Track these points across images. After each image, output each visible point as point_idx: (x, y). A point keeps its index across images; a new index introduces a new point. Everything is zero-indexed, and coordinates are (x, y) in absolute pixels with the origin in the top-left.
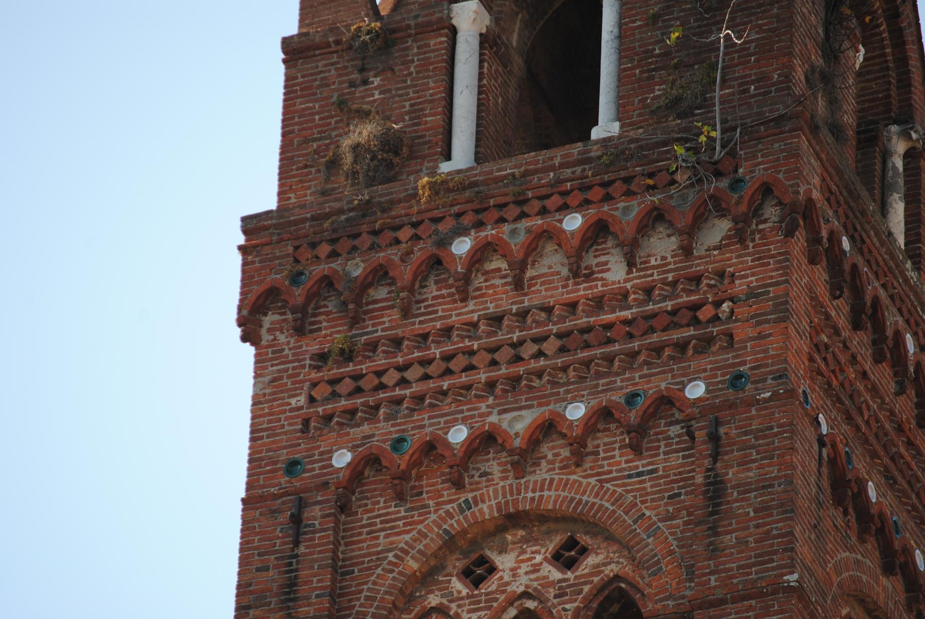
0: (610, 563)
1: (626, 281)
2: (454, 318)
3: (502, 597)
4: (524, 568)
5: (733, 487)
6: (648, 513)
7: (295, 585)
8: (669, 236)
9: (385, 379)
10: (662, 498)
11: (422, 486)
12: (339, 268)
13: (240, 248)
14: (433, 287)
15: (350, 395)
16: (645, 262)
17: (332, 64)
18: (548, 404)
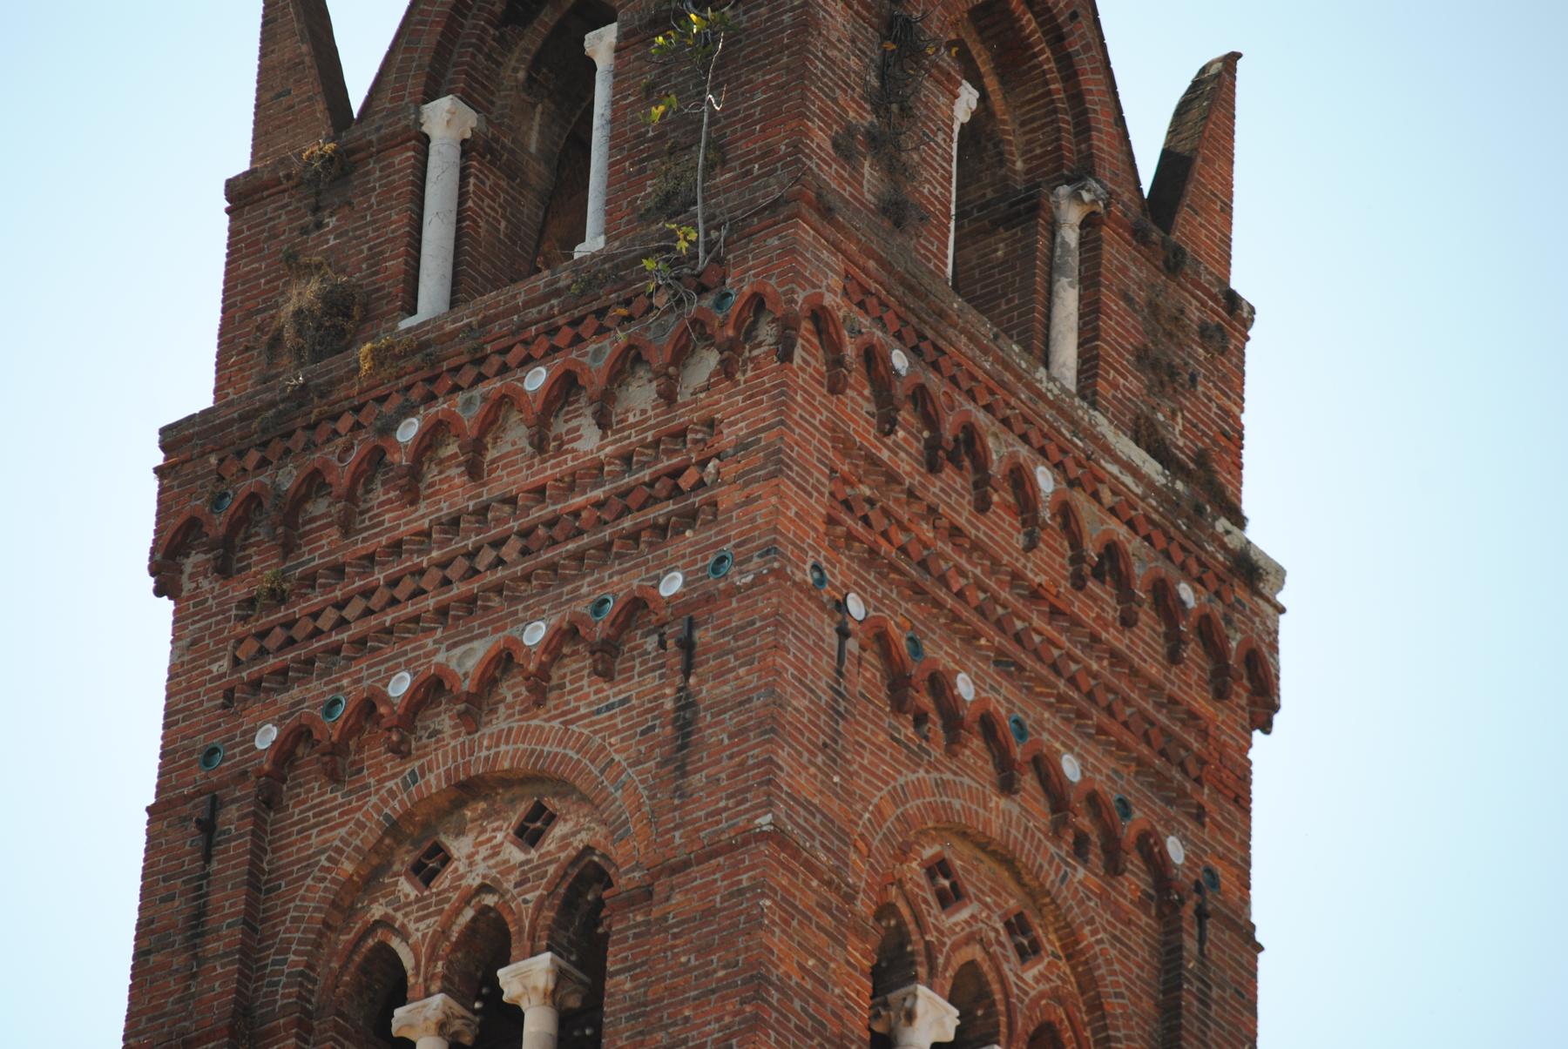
0: (579, 832)
1: (601, 448)
2: (402, 529)
3: (455, 896)
4: (484, 851)
5: (707, 709)
6: (617, 758)
7: (204, 914)
8: (650, 381)
9: (320, 623)
10: (632, 737)
11: (362, 760)
12: (268, 481)
13: (157, 470)
14: (380, 489)
15: (280, 649)
16: (622, 421)
17: (283, 207)
18: (504, 628)
